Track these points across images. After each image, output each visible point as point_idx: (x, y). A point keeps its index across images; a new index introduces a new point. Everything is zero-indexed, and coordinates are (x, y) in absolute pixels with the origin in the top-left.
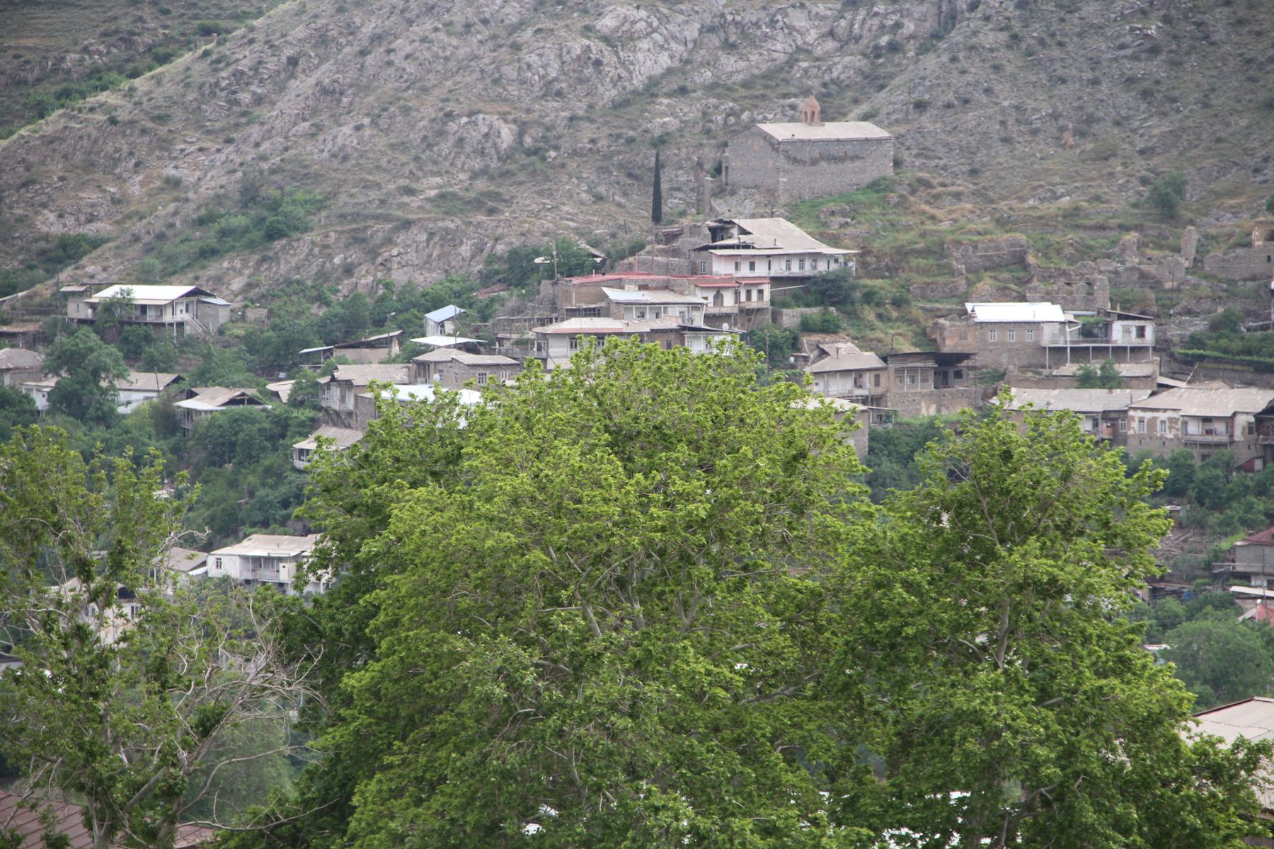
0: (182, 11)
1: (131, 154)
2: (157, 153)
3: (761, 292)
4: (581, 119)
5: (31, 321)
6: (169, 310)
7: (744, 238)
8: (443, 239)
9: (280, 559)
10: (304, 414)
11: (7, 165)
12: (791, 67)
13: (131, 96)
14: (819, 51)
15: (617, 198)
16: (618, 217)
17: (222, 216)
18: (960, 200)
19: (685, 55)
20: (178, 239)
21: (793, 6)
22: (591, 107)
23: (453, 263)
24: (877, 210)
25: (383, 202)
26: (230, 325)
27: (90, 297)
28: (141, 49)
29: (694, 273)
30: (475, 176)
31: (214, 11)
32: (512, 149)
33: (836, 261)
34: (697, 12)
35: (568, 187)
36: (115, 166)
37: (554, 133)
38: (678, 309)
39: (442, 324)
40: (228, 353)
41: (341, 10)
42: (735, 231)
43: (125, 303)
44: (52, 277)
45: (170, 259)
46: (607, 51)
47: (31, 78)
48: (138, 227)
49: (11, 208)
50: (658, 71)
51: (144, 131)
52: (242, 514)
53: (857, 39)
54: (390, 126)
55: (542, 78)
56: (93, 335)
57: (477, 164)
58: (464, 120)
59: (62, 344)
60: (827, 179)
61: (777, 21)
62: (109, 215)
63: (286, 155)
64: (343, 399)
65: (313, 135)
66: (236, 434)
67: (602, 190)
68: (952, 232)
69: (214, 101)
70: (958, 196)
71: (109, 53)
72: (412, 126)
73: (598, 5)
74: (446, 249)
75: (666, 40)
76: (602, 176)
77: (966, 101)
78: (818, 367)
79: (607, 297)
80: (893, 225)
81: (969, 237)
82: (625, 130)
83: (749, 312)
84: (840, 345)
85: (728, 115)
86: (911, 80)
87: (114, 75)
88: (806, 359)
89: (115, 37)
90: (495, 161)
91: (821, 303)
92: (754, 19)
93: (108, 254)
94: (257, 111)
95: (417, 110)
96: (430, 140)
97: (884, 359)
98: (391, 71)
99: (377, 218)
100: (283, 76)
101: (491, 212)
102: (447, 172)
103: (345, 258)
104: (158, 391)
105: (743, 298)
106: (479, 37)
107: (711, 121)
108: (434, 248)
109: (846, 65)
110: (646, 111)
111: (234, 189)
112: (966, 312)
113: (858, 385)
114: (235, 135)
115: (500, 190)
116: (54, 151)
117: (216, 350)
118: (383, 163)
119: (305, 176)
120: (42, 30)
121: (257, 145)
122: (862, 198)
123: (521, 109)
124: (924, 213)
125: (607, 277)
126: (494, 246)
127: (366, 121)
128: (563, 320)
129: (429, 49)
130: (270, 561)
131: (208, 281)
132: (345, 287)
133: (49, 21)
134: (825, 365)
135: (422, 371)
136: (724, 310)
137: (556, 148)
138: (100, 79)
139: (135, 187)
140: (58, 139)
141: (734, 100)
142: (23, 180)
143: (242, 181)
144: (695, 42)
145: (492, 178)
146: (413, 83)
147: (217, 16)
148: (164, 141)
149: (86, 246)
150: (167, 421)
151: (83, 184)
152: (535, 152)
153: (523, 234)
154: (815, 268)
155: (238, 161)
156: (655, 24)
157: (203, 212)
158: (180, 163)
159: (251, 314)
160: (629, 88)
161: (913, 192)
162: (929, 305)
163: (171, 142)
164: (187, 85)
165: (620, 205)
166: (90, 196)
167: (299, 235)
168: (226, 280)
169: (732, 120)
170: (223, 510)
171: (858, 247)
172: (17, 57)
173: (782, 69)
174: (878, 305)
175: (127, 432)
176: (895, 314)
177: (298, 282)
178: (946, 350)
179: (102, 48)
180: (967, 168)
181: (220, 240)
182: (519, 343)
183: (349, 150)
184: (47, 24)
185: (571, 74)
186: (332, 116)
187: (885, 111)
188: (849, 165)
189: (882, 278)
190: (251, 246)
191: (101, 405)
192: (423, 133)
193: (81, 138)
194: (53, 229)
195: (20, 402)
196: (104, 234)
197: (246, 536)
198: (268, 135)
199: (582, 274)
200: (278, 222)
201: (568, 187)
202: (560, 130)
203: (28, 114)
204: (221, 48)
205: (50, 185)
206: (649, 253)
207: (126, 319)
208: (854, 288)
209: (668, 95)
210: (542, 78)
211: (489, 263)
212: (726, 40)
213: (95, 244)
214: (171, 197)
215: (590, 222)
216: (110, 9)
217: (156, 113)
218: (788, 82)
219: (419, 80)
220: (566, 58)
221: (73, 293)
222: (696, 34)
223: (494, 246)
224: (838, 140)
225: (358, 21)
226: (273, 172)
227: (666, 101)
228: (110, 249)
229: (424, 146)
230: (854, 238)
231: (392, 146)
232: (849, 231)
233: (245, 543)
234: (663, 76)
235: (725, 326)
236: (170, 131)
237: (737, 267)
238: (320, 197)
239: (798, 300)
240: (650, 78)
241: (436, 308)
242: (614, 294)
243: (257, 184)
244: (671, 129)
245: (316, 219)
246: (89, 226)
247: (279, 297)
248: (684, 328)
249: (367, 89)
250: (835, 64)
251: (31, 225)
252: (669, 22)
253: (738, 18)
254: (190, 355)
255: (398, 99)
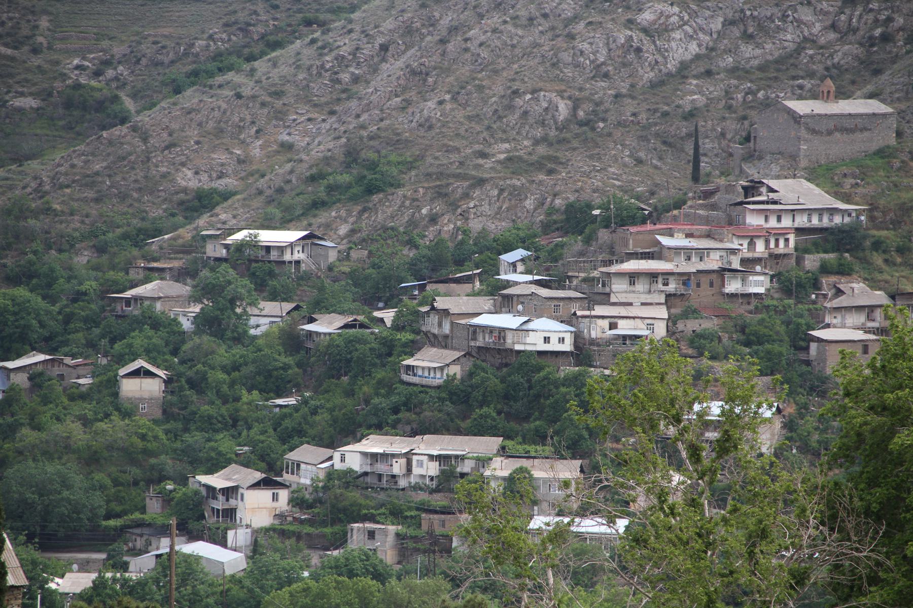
0: (289, 6)
1: (253, 123)
2: (274, 122)
3: (787, 240)
4: (625, 96)
5: (175, 259)
6: (289, 251)
7: (772, 195)
8: (510, 194)
9: (393, 456)
11: (154, 131)
12: (799, 54)
14: (822, 41)
15: (654, 161)
17: (330, 174)
19: (711, 44)
20: (294, 193)
21: (801, 4)
22: (632, 86)
23: (519, 214)
24: (882, 173)
25: (461, 163)
26: (337, 263)
27: (225, 239)
28: (256, 37)
30: (537, 142)
31: (315, 6)
32: (567, 121)
33: (850, 215)
34: (721, 8)
35: (613, 152)
36: (240, 132)
38: (719, 253)
39: (514, 265)
40: (337, 286)
41: (423, 6)
42: (764, 190)
44: (190, 223)
45: (288, 209)
46: (646, 41)
47: (166, 60)
48: (262, 183)
49: (157, 166)
50: (688, 57)
51: (263, 104)
52: (359, 419)
53: (855, 31)
55: (592, 62)
56: (231, 270)
57: (539, 133)
60: (841, 147)
61: (788, 16)
62: (236, 172)
63: (382, 125)
64: (440, 325)
65: (404, 108)
66: (350, 353)
67: (642, 155)
71: (229, 40)
72: (485, 101)
73: (639, 2)
74: (513, 202)
75: (695, 31)
76: (642, 143)
78: (836, 303)
79: (660, 243)
80: (896, 186)
82: (660, 106)
84: (854, 285)
85: (747, 94)
87: (234, 59)
88: (825, 296)
89: (235, 28)
91: (838, 250)
92: (769, 14)
93: (236, 205)
94: (355, 88)
95: (490, 88)
96: (501, 113)
97: (893, 297)
98: (467, 56)
99: (458, 176)
100: (376, 59)
101: (550, 172)
102: (514, 139)
103: (431, 209)
104: (281, 317)
105: (772, 245)
106: (540, 28)
107: (733, 99)
108: (504, 202)
109: (846, 53)
110: (678, 90)
111: (339, 154)
113: (870, 318)
114: (337, 108)
115: (558, 154)
116: (191, 120)
118: (462, 131)
119: (397, 142)
120: (175, 21)
121: (358, 116)
122: (869, 162)
125: (658, 226)
126: (553, 201)
128: (622, 262)
129: (499, 38)
130: (385, 457)
131: (319, 227)
133: (181, 14)
135: (506, 303)
136: (756, 255)
137: (604, 120)
139: (256, 150)
140: (194, 110)
141: (751, 81)
142: (166, 143)
143: (346, 145)
144: (719, 33)
145: (551, 145)
146: (486, 66)
147: (317, 11)
148: (280, 112)
149: (217, 198)
150: (293, 341)
151: (215, 147)
152: (586, 123)
153: (577, 191)
154: (831, 220)
155: (343, 129)
156: (686, 18)
157: (314, 170)
158: (292, 130)
159: (354, 255)
160: (664, 70)
163: (286, 114)
164: (298, 67)
165: (656, 167)
166: (220, 157)
167: (394, 191)
168: (334, 226)
169: (750, 97)
170: (344, 414)
171: (867, 204)
172: (155, 43)
173: (791, 56)
174: (884, 252)
176: (899, 260)
177: (392, 229)
179: (224, 36)
181: (328, 194)
182: (585, 280)
183: (434, 121)
184: (179, 17)
185: (617, 59)
186: (419, 93)
187: (888, 90)
188: (859, 136)
189: (888, 229)
190: (354, 199)
191: (236, 327)
192: (495, 107)
193: (212, 109)
194: (191, 184)
195: (170, 324)
196: (231, 188)
198: (367, 108)
199: (634, 224)
200: (376, 179)
201: (613, 152)
202: (607, 105)
203: (165, 90)
204: (325, 37)
206: (691, 207)
207: (252, 258)
208: (865, 237)
209: (696, 77)
210: (592, 62)
211: (549, 214)
212: (745, 31)
213: (226, 196)
214: (286, 159)
215: (633, 181)
216: (230, 4)
217: (273, 89)
218: (796, 66)
219: (492, 63)
220: (613, 46)
221: (210, 236)
222: (720, 26)
223: (553, 201)
224: (850, 114)
225: (437, 15)
226: (371, 138)
227: (695, 82)
228: (238, 200)
229: (495, 118)
230: (864, 196)
232: (860, 190)
233: (364, 442)
236: (284, 104)
237: (766, 220)
238: (409, 159)
239: (817, 247)
240: (681, 63)
241: (506, 252)
242: (665, 241)
243: (359, 149)
246: (220, 182)
247: (377, 241)
248: (724, 270)
249: (448, 71)
250: (836, 51)
251: (173, 181)
252: (697, 16)
253: (756, 13)
254: (306, 288)
255: (474, 79)
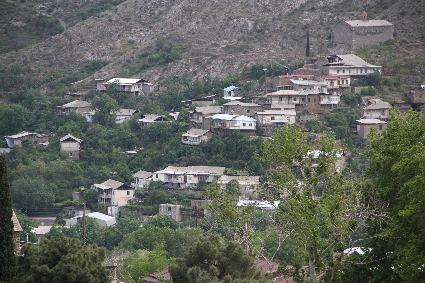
1: (117, 32)
2: (126, 32)
3: (347, 81)
4: (277, 19)
5: (84, 91)
7: (340, 62)
8: (228, 62)
10: (183, 124)
13: (116, 11)
15: (290, 47)
16: (290, 54)
17: (150, 54)
18: (418, 48)
20: (135, 62)
22: (280, 15)
23: (232, 71)
24: (388, 51)
25: (207, 49)
26: (154, 92)
27: (105, 82)
29: (323, 74)
30: (239, 40)
33: (374, 70)
36: (111, 36)
37: (267, 24)
38: (318, 87)
39: (230, 93)
43: (117, 84)
44: (90, 76)
45: (132, 69)
47: (79, 5)
48: (121, 58)
49: (76, 51)
51: (121, 24)
54: (209, 22)
55: (263, 5)
56: (108, 96)
57: (240, 35)
58: (235, 20)
59: (98, 99)
62: (109, 53)
63: (173, 32)
64: (198, 119)
65: (182, 25)
66: (160, 131)
67: (284, 44)
68: (416, 59)
69: (145, 13)
70: (417, 46)
72: (217, 22)
76: (284, 39)
77: (420, 12)
78: (368, 108)
79: (292, 83)
80: (394, 57)
81: (422, 61)
82: (292, 23)
83: (343, 88)
84: (376, 100)
85: (329, 18)
86: (400, 5)
88: (363, 105)
90: (246, 34)
91: (369, 85)
93: (110, 68)
94: (160, 17)
95: (219, 16)
96: (223, 27)
97: (392, 105)
99: (205, 55)
100: (169, 4)
101: (245, 52)
102: (229, 38)
103: (194, 69)
104: (130, 116)
105: (341, 83)
107: (323, 20)
108: (225, 65)
110: (300, 16)
111: (154, 46)
112: (421, 88)
113: (383, 114)
114: (153, 25)
117: (149, 101)
118: (207, 35)
119: (179, 40)
121: (162, 29)
123: (255, 16)
124: (405, 52)
125: (292, 75)
126: (246, 65)
127: (200, 20)
128: (276, 91)
130: (175, 175)
131: (146, 77)
132: (194, 79)
134: (371, 107)
135: (226, 109)
136: (334, 88)
137: (268, 30)
138: (103, 5)
139: (118, 44)
140: (91, 27)
141: (331, 12)
142: (79, 41)
143: (157, 41)
145: (245, 40)
148: (128, 27)
149: (101, 65)
150: (135, 126)
151: (100, 43)
153: (257, 61)
154: (366, 72)
155: (155, 34)
157: (143, 52)
158: (134, 35)
159: (161, 89)
161: (401, 45)
162: (407, 86)
163: (131, 28)
165: (291, 50)
166: (103, 47)
168: (152, 77)
169: (331, 19)
170: (157, 157)
171: (381, 65)
174: (389, 85)
175: (121, 130)
176: (395, 89)
177: (177, 77)
178: (414, 102)
180: (420, 36)
182: (260, 99)
185: (273, 3)
187: (390, 16)
188: (378, 35)
190: (161, 65)
192: (221, 24)
194: (90, 58)
195: (82, 119)
196: (107, 60)
197: (165, 167)
198: (166, 25)
199: (281, 74)
201: (272, 44)
202: (269, 23)
205: (89, 43)
206: (306, 67)
207: (117, 90)
208: (380, 79)
209: (307, 11)
210: (263, 5)
211: (244, 71)
215: (281, 56)
217: (125, 17)
218: (351, 6)
219: (220, 6)
221: (99, 81)
223: (246, 65)
224: (374, 26)
226: (168, 38)
227: (307, 13)
228: (111, 66)
229: (221, 29)
230: (380, 62)
231: (210, 29)
232: (378, 59)
233: (166, 169)
234: (306, 4)
235: (335, 93)
236: (130, 24)
237: (338, 72)
238: (184, 47)
239: (360, 84)
240: (301, 5)
241: (226, 87)
242: (295, 82)
244: (309, 23)
245: (183, 55)
246: (103, 58)
247: (171, 83)
248: (320, 94)
249: (201, 9)
251: (83, 57)
254: (140, 103)
255: (212, 12)
